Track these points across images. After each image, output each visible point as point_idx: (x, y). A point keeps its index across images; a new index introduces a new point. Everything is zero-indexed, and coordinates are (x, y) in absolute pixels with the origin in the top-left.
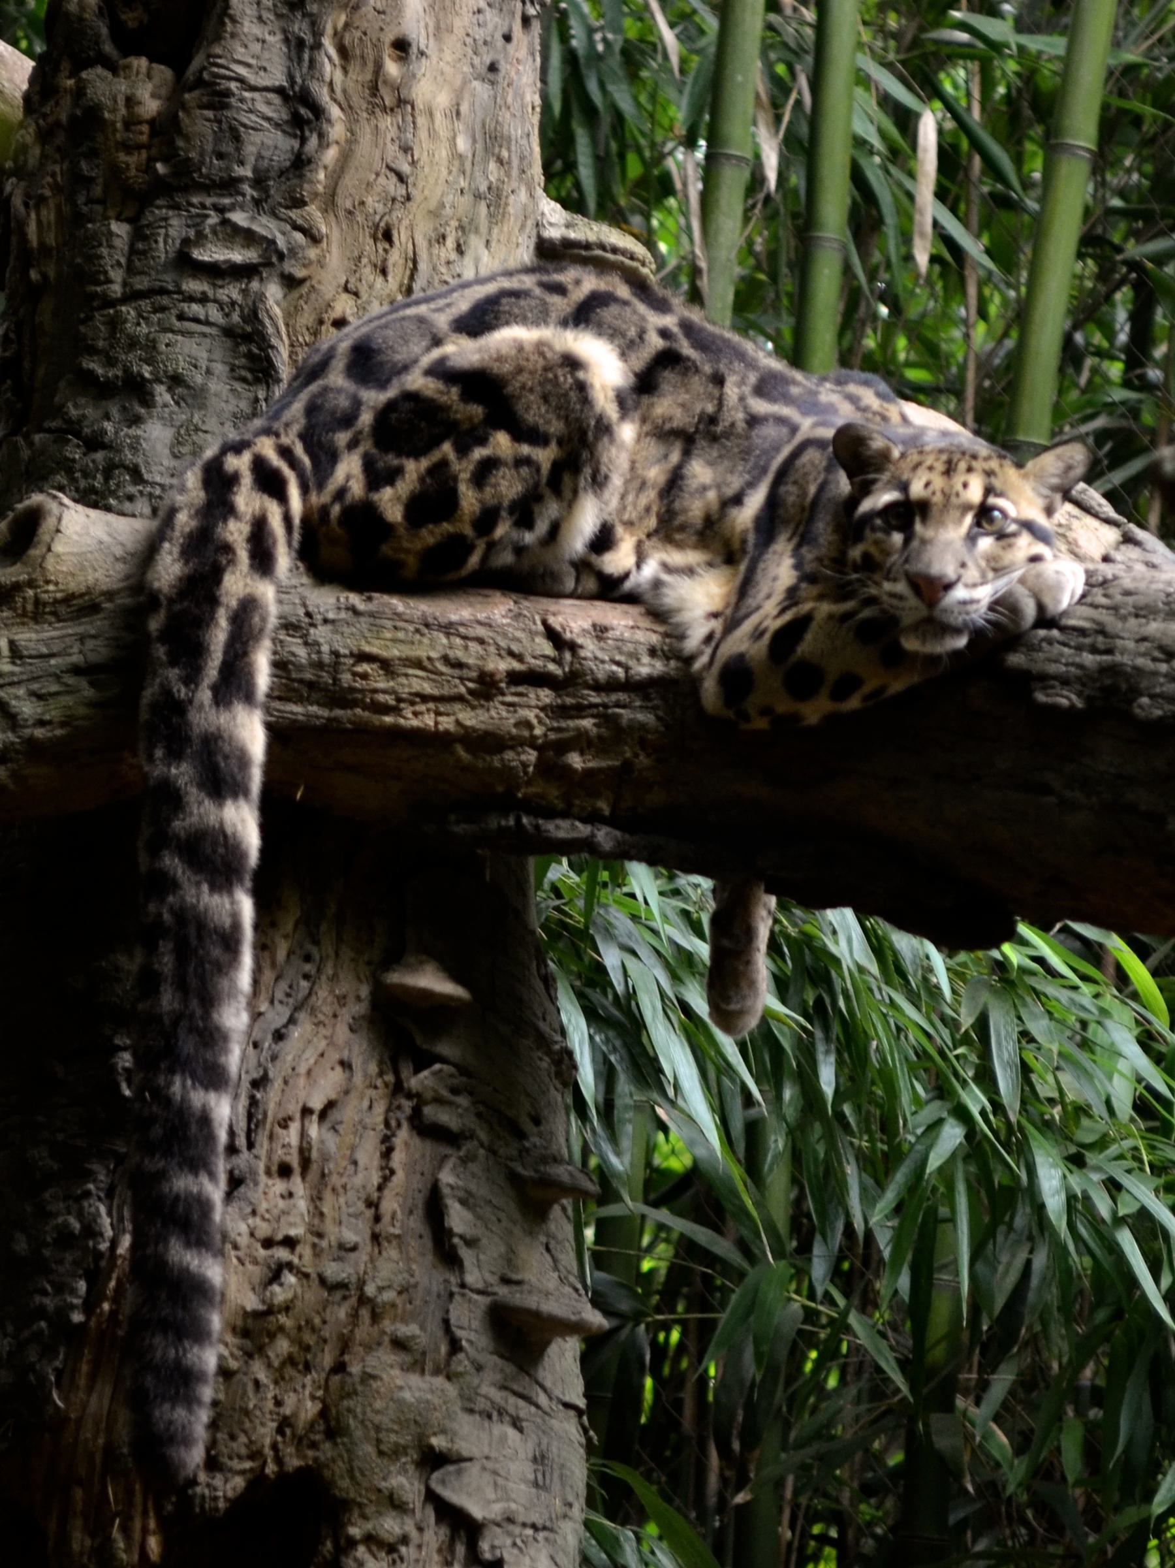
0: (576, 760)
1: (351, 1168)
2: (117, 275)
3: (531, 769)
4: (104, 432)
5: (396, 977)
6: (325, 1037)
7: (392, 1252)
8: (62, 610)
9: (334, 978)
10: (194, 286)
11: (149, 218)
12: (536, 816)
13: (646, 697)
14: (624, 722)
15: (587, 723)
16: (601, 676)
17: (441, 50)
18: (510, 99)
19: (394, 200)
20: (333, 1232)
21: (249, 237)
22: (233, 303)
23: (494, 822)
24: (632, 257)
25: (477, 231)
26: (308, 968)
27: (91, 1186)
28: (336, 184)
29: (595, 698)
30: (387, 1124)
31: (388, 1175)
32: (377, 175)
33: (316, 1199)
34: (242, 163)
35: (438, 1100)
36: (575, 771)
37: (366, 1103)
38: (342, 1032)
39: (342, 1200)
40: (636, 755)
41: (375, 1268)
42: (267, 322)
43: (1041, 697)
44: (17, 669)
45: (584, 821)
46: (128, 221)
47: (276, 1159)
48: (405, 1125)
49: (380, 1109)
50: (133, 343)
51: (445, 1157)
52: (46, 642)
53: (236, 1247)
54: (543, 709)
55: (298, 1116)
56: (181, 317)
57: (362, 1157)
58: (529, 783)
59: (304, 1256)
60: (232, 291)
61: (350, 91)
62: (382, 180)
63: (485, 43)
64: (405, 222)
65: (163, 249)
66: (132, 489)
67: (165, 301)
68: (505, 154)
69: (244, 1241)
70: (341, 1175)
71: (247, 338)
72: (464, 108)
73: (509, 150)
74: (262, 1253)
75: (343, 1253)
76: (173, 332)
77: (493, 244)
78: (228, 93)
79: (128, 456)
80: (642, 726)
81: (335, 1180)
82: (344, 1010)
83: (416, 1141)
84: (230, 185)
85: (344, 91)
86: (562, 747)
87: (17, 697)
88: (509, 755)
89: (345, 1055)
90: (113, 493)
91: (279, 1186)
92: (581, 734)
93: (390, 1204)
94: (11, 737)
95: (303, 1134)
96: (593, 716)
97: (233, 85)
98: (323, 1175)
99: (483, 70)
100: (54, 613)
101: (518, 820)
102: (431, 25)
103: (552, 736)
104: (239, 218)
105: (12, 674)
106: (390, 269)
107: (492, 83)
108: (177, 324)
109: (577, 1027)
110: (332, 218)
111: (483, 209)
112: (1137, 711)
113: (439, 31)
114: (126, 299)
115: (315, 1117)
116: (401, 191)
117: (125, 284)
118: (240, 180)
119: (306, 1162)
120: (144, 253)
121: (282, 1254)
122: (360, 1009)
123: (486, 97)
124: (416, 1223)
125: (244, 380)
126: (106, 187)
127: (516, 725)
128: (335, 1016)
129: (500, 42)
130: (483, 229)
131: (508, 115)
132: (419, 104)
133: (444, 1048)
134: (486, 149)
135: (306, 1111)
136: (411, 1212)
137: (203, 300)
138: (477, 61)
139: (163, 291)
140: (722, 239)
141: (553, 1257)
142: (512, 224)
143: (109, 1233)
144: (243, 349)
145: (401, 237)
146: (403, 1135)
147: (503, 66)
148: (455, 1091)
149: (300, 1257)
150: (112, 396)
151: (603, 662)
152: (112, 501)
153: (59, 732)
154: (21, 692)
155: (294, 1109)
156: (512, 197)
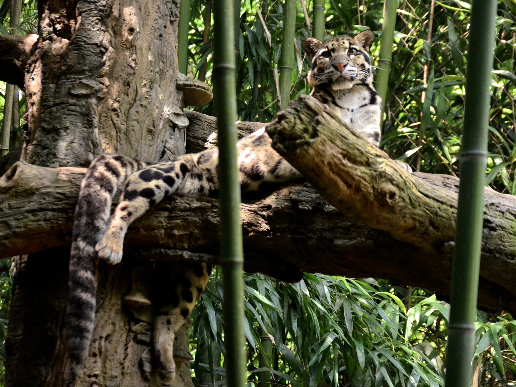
0: (176, 232)
1: (115, 354)
2: (51, 99)
3: (163, 235)
4: (47, 144)
5: (128, 298)
6: (107, 316)
7: (128, 378)
8: (23, 194)
9: (111, 299)
10: (72, 101)
11: (60, 82)
12: (166, 249)
13: (196, 213)
14: (189, 220)
15: (179, 221)
16: (182, 207)
17: (144, 31)
18: (166, 45)
19: (130, 74)
20: (109, 373)
21: (87, 86)
22: (83, 105)
23: (153, 251)
24: (204, 88)
25: (156, 82)
26: (102, 296)
27: (40, 362)
28: (113, 71)
29: (180, 214)
30: (126, 341)
31: (126, 355)
32: (125, 67)
33: (104, 363)
34: (85, 65)
35: (142, 333)
36: (176, 235)
37: (120, 335)
38: (113, 314)
39: (113, 363)
40: (194, 230)
41: (122, 382)
42: (92, 110)
43: (300, 207)
44: (10, 212)
45: (180, 250)
46: (55, 84)
47: (92, 352)
48: (132, 340)
49: (124, 337)
50: (55, 118)
51: (145, 350)
52: (19, 204)
53: (80, 378)
54: (165, 217)
55: (98, 339)
56: (68, 110)
57: (119, 350)
58: (163, 239)
59: (101, 380)
60: (83, 102)
61: (117, 44)
62: (126, 69)
63: (158, 29)
64: (134, 81)
65: (64, 91)
66: (53, 160)
67: (64, 106)
68: (165, 60)
69: (82, 376)
70: (112, 356)
71: (87, 115)
72: (152, 47)
73: (166, 59)
74: (88, 379)
75: (113, 379)
76: (66, 114)
77: (162, 86)
78: (81, 46)
79: (53, 151)
80: (195, 222)
81: (110, 357)
82: (113, 308)
83: (136, 345)
84: (82, 72)
85: (115, 44)
86: (172, 228)
87: (11, 220)
88: (156, 231)
89: (114, 321)
90: (48, 161)
91: (93, 359)
92: (177, 224)
93: (127, 364)
94: (8, 231)
95: (100, 344)
96: (180, 219)
97: (82, 43)
98: (106, 356)
99: (157, 36)
100: (21, 195)
101: (160, 250)
102: (141, 24)
103: (169, 225)
104: (84, 81)
105: (9, 213)
106: (129, 94)
107: (161, 40)
108: (68, 112)
109: (212, 313)
110: (112, 80)
111: (157, 76)
112: (325, 209)
113: (143, 25)
114: (53, 106)
115: (103, 339)
116: (132, 71)
117: (54, 102)
118: (85, 70)
119: (100, 352)
120: (58, 92)
121: (93, 379)
122: (119, 307)
123: (159, 44)
124: (136, 369)
125: (86, 127)
126: (49, 74)
127: (158, 222)
128: (111, 310)
129: (163, 28)
130: (158, 81)
131: (166, 49)
132: (138, 47)
133: (143, 318)
134: (159, 59)
135: (101, 338)
136: (134, 366)
137: (74, 105)
138: (156, 34)
139: (63, 103)
140: (285, 91)
141: (182, 378)
142: (167, 80)
143: (45, 375)
144: (86, 118)
145: (133, 85)
146: (131, 343)
147: (164, 35)
148: (147, 330)
149: (99, 380)
150: (50, 134)
151: (183, 203)
152: (48, 164)
153: (23, 229)
154: (12, 218)
155: (97, 337)
156: (167, 73)
